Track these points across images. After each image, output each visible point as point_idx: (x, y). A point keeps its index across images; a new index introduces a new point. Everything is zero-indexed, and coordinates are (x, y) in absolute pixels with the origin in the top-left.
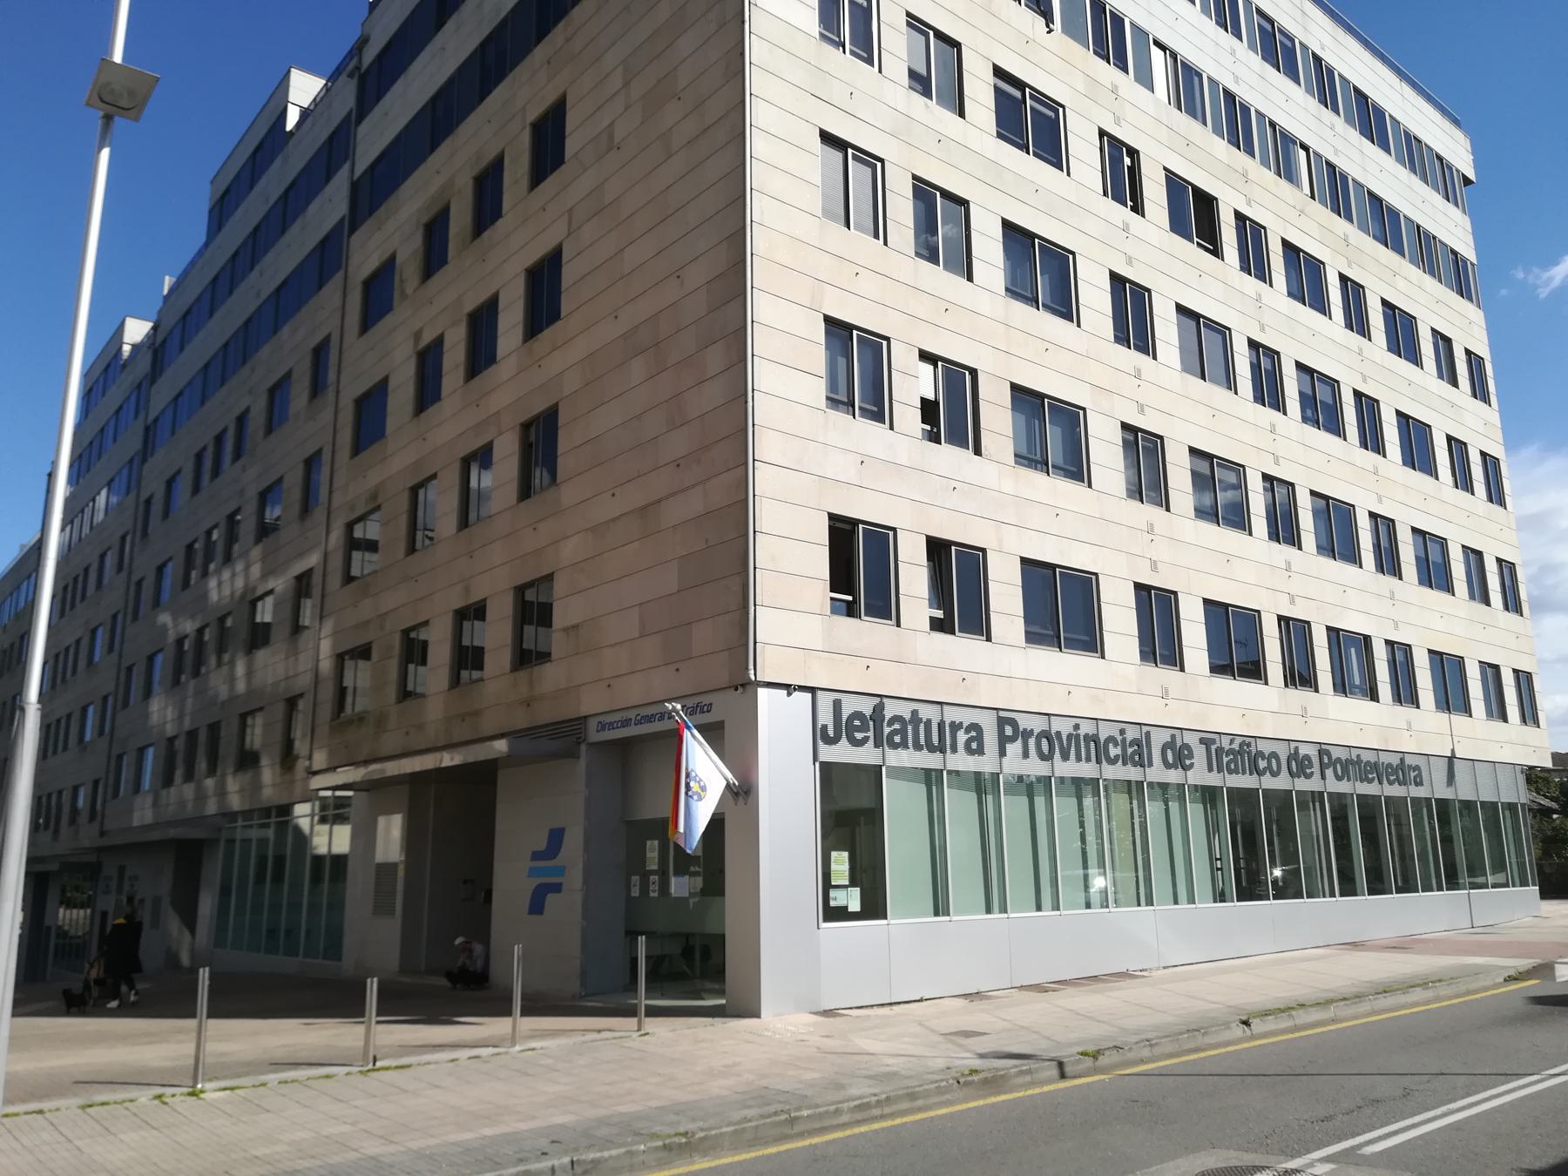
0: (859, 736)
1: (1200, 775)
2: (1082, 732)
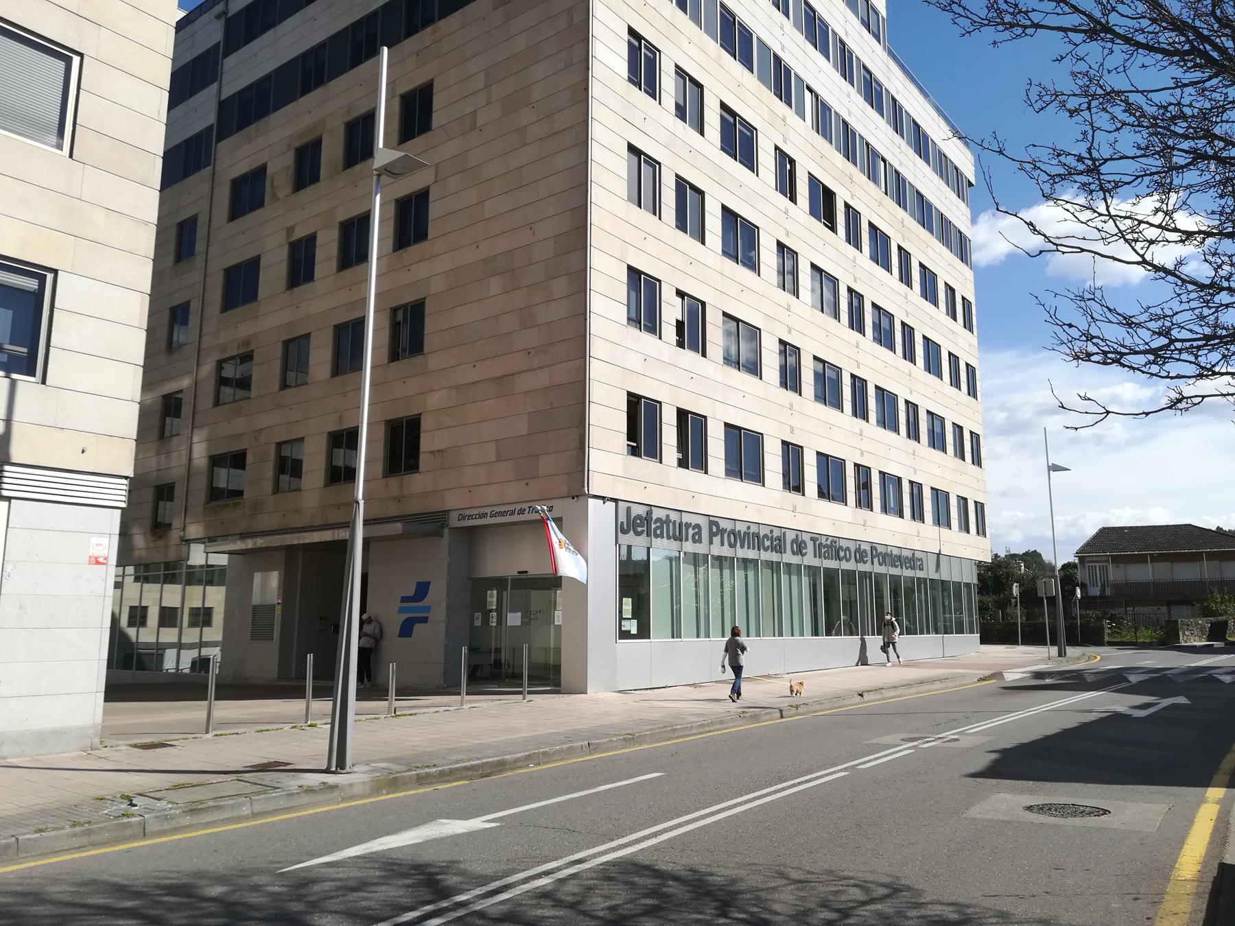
0: (639, 529)
1: (810, 560)
2: (751, 531)
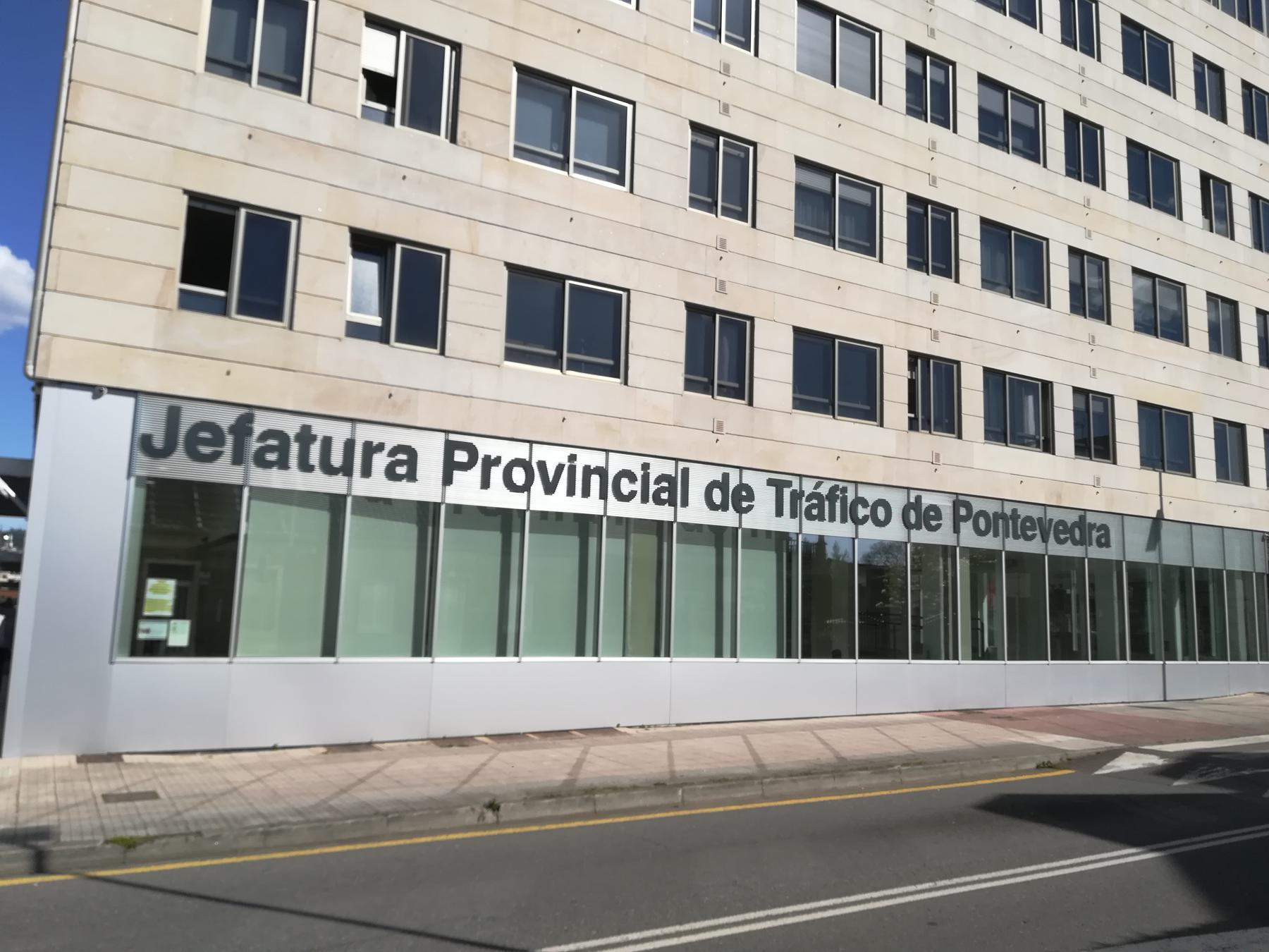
0: (1029, 533)
1: (762, 516)
